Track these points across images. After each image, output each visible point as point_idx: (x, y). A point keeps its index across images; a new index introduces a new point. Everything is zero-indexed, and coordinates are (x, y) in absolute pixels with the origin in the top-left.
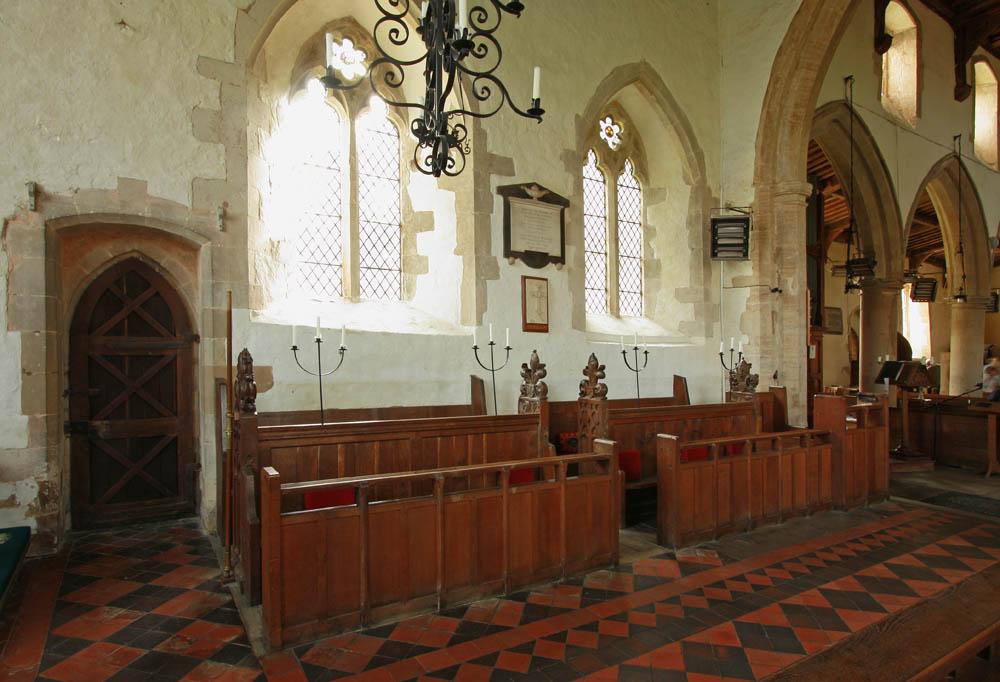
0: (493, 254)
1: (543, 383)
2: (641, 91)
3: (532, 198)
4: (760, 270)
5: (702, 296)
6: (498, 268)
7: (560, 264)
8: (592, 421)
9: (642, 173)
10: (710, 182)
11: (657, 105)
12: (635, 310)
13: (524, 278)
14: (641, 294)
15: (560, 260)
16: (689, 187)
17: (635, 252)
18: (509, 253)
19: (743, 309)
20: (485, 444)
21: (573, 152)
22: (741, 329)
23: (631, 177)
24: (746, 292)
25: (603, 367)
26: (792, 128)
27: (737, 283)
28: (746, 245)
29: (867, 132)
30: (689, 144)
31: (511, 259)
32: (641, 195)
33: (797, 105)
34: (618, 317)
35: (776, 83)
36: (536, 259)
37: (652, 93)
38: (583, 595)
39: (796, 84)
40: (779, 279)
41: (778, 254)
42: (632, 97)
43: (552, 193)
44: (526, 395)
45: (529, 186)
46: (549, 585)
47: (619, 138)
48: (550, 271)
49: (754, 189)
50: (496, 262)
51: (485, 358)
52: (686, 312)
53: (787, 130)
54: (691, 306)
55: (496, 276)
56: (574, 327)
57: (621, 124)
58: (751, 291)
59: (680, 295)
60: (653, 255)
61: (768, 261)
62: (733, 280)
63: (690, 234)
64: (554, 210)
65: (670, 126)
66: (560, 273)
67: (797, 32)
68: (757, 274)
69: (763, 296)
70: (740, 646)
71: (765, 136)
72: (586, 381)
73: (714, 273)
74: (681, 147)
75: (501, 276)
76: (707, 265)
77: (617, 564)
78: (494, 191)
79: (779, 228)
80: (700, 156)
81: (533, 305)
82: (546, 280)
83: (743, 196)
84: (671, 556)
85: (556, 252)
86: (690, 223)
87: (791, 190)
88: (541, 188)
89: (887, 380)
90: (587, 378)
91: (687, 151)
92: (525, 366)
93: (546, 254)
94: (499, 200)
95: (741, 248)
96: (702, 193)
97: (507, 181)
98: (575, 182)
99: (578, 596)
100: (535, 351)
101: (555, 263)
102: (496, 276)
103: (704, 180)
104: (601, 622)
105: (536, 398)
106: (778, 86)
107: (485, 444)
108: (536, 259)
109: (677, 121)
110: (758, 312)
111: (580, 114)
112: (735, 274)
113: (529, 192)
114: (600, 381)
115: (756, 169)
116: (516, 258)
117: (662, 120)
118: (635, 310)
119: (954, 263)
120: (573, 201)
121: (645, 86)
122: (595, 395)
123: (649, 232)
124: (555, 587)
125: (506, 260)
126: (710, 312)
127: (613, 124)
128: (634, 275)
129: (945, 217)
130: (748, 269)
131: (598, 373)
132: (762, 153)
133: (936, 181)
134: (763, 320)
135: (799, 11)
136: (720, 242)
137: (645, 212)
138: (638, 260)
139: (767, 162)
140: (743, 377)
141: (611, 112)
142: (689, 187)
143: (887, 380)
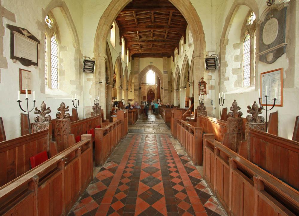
0: (4, 56)
1: (49, 116)
2: (61, 11)
3: (24, 35)
4: (95, 77)
5: (79, 83)
6: (7, 63)
7: (36, 66)
8: (63, 128)
9: (59, 39)
10: (81, 49)
11: (67, 19)
12: (56, 86)
13: (21, 70)
14: (58, 81)
15: (36, 64)
16: (75, 48)
17: (56, 66)
18: (13, 57)
19: (90, 88)
20: (24, 149)
21: (41, 23)
22: (89, 93)
23: (55, 40)
24: (91, 83)
25: (49, 108)
26: (103, 40)
27: (88, 80)
28: (93, 69)
29: (109, 47)
30: (76, 35)
31: (15, 60)
32: (58, 47)
33: (104, 34)
34: (51, 89)
35: (100, 26)
36: (26, 62)
37: (66, 14)
38: (94, 199)
39: (104, 28)
40: (100, 80)
41: (100, 72)
42: (57, 12)
43: (33, 36)
44: (38, 122)
45: (24, 29)
46: (77, 203)
47: (51, 24)
48: (32, 68)
49: (94, 54)
50: (6, 61)
51: (24, 107)
52: (74, 88)
53: (102, 40)
54: (75, 86)
55: (6, 67)
56: (41, 92)
57: (52, 20)
58: (93, 82)
59: (71, 82)
60: (62, 68)
61: (97, 75)
62: (87, 79)
63: (75, 63)
64: (34, 43)
65: (70, 27)
66: (36, 70)
67: (106, 15)
68: (95, 78)
69: (96, 84)
70: (150, 188)
71: (97, 39)
72: (59, 113)
73: (82, 76)
74: (73, 35)
75: (9, 67)
76: (80, 73)
77: (92, 180)
78: (5, 26)
79: (99, 66)
80: (78, 39)
81: (24, 81)
82: (30, 72)
83: (91, 56)
84: (103, 169)
85: (35, 61)
86: (75, 60)
87: (103, 56)
88: (29, 32)
89: (116, 106)
90: (60, 112)
91: (75, 36)
92: (249, 107)
93: (30, 61)
94: (8, 32)
95: (91, 70)
96: (78, 51)
97: (12, 24)
98: (41, 35)
99: (93, 200)
100: (43, 102)
101: (34, 65)
102: (6, 67)
103: (79, 47)
104: (112, 206)
105: (46, 123)
106: (100, 27)
107: (24, 149)
108: (26, 62)
109: (73, 26)
110: (95, 89)
111: (44, 9)
112: (88, 77)
113: (23, 32)
114: (66, 112)
115: (94, 48)
116: (17, 60)
117: (67, 24)
118: (56, 86)
119: (118, 80)
120: (41, 42)
121: (64, 10)
122: (65, 118)
123: (61, 61)
124: (80, 202)
125: (11, 60)
126: (81, 88)
127: (49, 19)
128: (55, 75)
129: (117, 70)
130: (91, 76)
131: (66, 110)
132: (96, 44)
133: (272, 53)
134: (96, 91)
135: (106, 9)
136: (86, 67)
137: (59, 53)
138: (57, 69)
139: (97, 47)
140: (97, 107)
141: (49, 14)
142: (75, 48)
143: (116, 106)
